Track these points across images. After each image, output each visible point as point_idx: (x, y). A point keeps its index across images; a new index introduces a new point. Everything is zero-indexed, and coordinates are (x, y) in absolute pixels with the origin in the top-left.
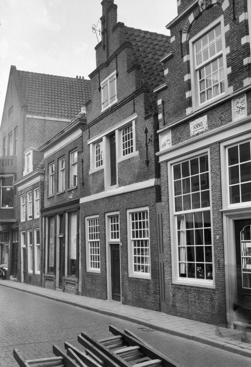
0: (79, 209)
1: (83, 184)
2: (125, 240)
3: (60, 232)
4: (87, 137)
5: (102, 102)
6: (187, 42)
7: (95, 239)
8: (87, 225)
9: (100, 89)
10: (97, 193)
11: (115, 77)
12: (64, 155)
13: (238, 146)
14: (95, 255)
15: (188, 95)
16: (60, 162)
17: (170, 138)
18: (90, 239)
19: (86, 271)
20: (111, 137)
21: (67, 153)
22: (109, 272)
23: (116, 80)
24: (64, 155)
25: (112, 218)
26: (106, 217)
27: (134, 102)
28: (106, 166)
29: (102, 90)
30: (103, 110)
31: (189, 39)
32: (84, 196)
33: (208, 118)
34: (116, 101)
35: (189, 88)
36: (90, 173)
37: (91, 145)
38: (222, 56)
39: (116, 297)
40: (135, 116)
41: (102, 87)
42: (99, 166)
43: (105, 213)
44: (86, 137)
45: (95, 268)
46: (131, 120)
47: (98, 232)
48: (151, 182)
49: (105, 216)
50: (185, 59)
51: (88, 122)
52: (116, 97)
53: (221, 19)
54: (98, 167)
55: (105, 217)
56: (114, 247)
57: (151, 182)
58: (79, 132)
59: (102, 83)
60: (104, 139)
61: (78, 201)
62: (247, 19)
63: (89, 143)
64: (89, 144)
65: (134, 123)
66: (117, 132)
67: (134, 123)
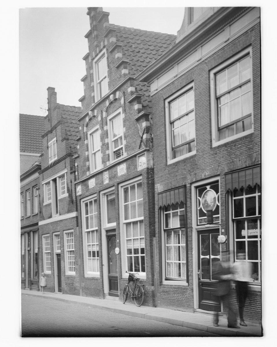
0: (38, 229)
1: (40, 212)
2: (63, 251)
3: (28, 247)
4: (42, 180)
5: (49, 157)
6: (106, 118)
7: (69, 249)
8: (65, 237)
9: (48, 147)
10: (68, 213)
11: (56, 142)
12: (29, 189)
13: (88, 202)
14: (49, 262)
15: (87, 163)
16: (28, 193)
17: (81, 188)
18: (68, 249)
19: (84, 277)
20: (55, 180)
21: (25, 191)
22: (196, 278)
23: (56, 144)
24: (29, 189)
25: (67, 234)
26: (54, 236)
27: (65, 161)
28: (52, 201)
29: (49, 148)
30: (50, 162)
31: (108, 116)
32: (41, 220)
33: (96, 179)
34: (56, 158)
35: (88, 160)
36: (44, 204)
37: (44, 185)
38: (21, 193)
39: (60, 290)
40: (65, 171)
41: (49, 146)
42: (63, 194)
43: (53, 233)
44: (41, 179)
45: (70, 272)
46: (64, 173)
47: (60, 245)
48: (74, 214)
49: (53, 235)
50: (86, 142)
51: (42, 169)
52: (56, 155)
53: (120, 110)
54: (49, 201)
55: (53, 236)
56: (58, 255)
57: (74, 214)
58: (36, 175)
59: (49, 143)
60: (51, 182)
61: (37, 224)
62: (87, 143)
63: (43, 184)
64: (43, 184)
65: (65, 174)
66: (57, 179)
67: (65, 174)
